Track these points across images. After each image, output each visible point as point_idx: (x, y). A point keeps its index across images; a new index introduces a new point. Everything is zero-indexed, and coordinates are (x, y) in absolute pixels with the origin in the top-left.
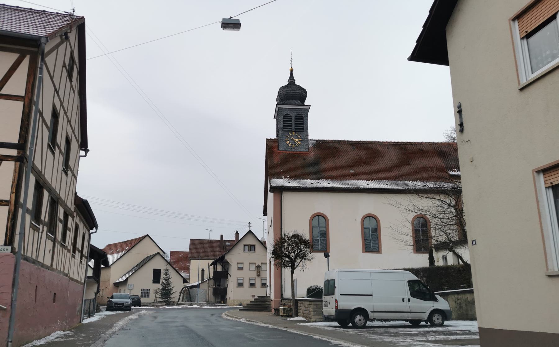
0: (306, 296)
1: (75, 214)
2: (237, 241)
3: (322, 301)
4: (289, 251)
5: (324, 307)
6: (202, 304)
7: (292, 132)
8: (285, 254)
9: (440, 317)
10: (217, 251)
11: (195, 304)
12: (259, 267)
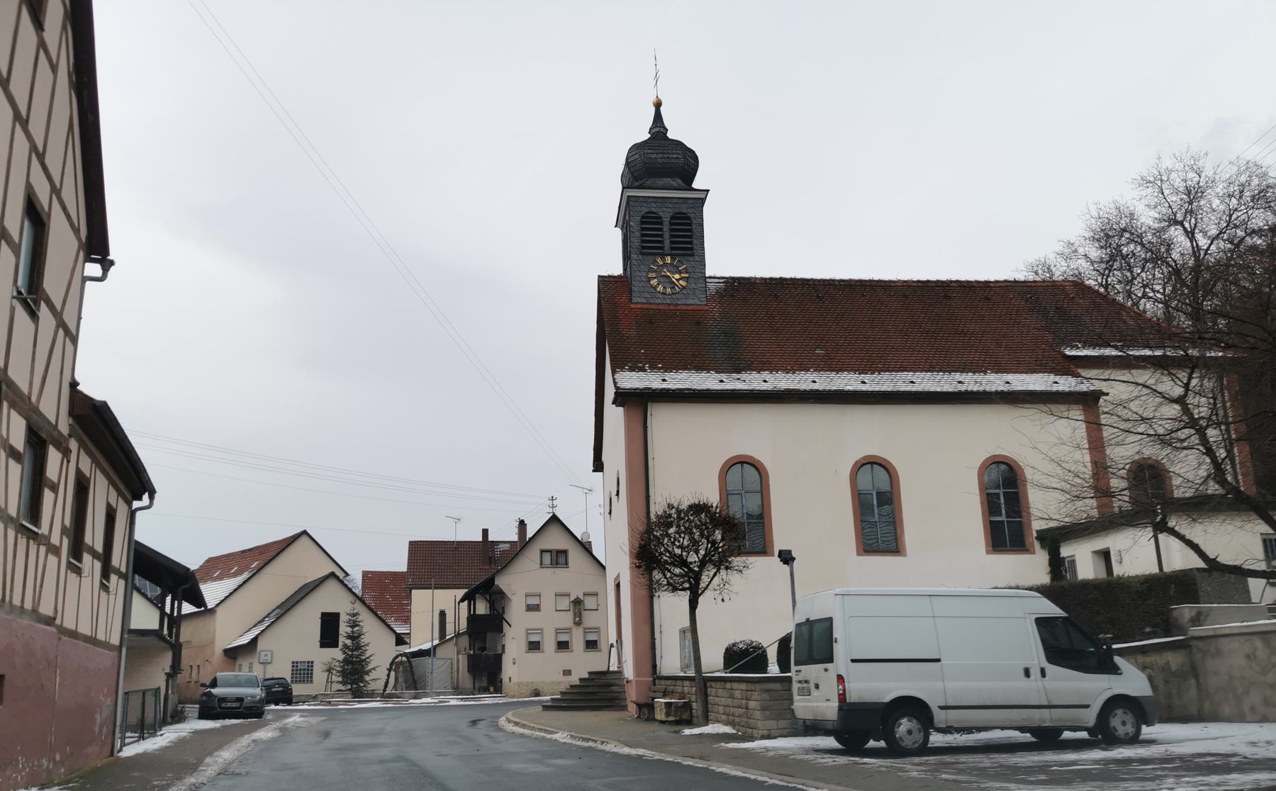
0: (721, 666)
1: (73, 445)
2: (523, 543)
4: (695, 542)
5: (796, 697)
6: (444, 694)
7: (663, 256)
8: (673, 555)
9: (1130, 719)
10: (474, 569)
12: (577, 602)
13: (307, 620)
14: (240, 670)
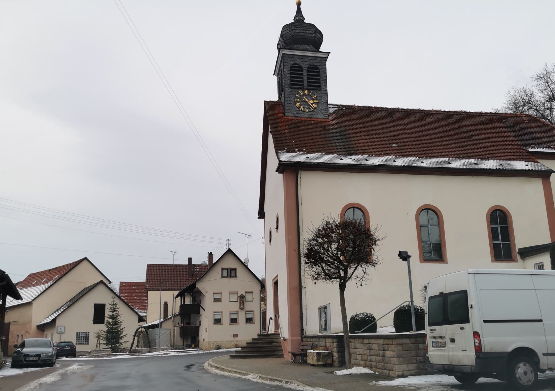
2: (212, 265)
3: (424, 336)
5: (430, 348)
6: (166, 349)
7: (303, 90)
10: (184, 280)
11: (156, 350)
12: (242, 297)
13: (86, 308)
14: (46, 337)
